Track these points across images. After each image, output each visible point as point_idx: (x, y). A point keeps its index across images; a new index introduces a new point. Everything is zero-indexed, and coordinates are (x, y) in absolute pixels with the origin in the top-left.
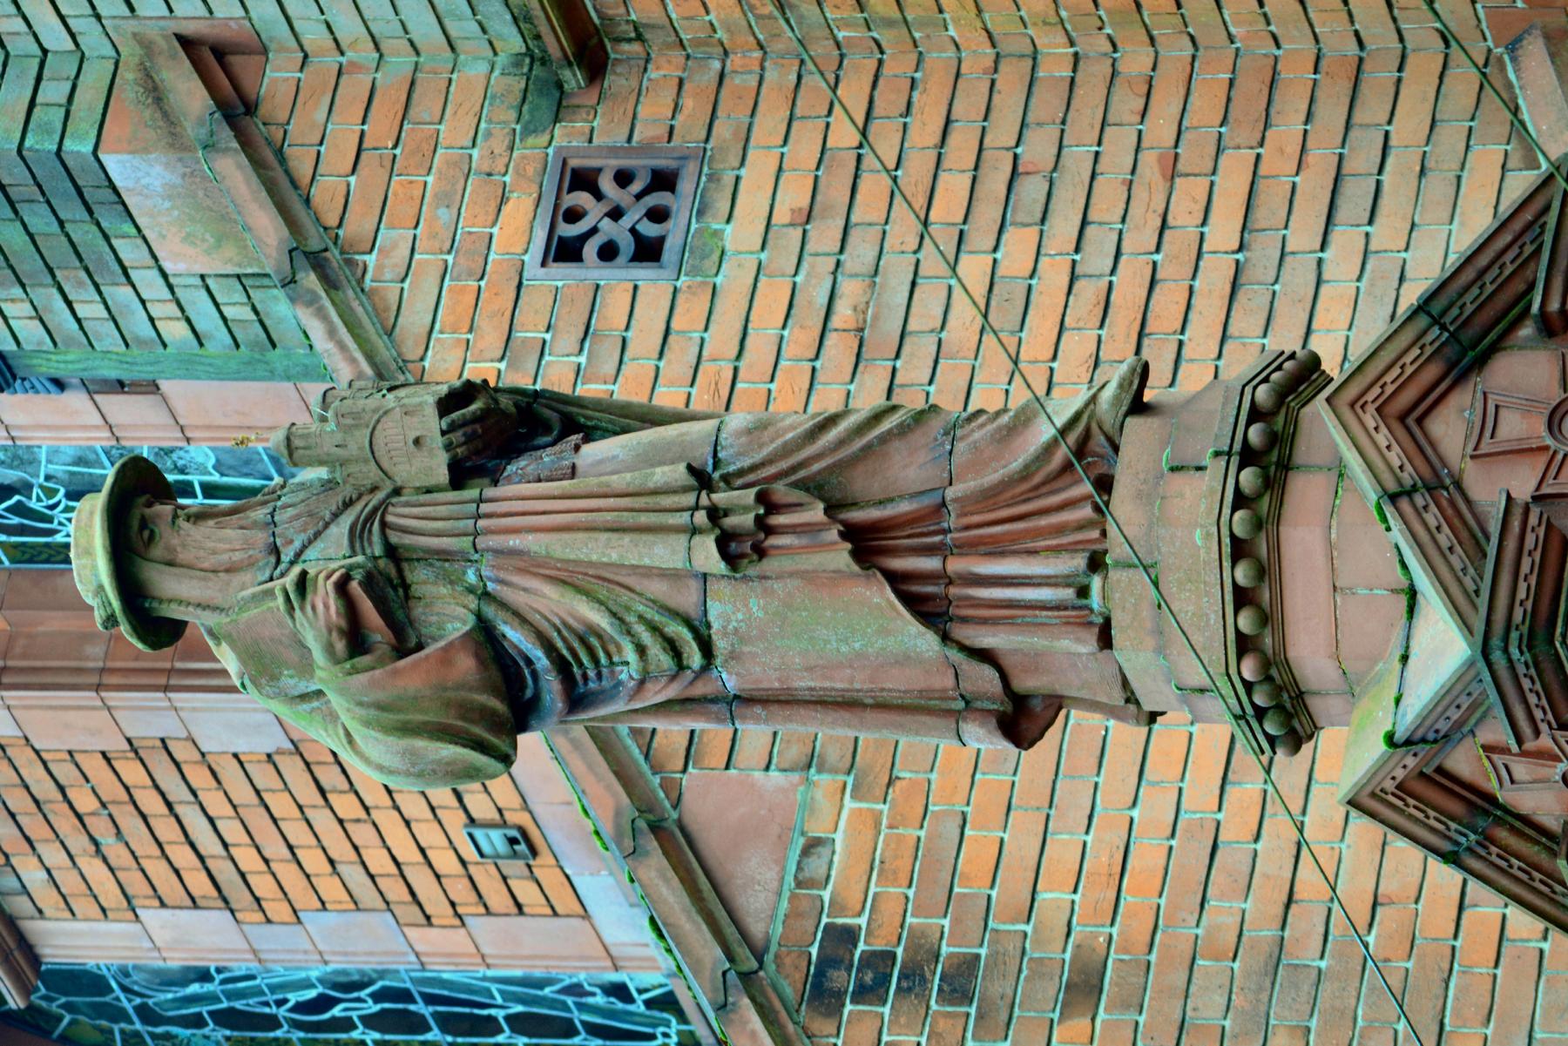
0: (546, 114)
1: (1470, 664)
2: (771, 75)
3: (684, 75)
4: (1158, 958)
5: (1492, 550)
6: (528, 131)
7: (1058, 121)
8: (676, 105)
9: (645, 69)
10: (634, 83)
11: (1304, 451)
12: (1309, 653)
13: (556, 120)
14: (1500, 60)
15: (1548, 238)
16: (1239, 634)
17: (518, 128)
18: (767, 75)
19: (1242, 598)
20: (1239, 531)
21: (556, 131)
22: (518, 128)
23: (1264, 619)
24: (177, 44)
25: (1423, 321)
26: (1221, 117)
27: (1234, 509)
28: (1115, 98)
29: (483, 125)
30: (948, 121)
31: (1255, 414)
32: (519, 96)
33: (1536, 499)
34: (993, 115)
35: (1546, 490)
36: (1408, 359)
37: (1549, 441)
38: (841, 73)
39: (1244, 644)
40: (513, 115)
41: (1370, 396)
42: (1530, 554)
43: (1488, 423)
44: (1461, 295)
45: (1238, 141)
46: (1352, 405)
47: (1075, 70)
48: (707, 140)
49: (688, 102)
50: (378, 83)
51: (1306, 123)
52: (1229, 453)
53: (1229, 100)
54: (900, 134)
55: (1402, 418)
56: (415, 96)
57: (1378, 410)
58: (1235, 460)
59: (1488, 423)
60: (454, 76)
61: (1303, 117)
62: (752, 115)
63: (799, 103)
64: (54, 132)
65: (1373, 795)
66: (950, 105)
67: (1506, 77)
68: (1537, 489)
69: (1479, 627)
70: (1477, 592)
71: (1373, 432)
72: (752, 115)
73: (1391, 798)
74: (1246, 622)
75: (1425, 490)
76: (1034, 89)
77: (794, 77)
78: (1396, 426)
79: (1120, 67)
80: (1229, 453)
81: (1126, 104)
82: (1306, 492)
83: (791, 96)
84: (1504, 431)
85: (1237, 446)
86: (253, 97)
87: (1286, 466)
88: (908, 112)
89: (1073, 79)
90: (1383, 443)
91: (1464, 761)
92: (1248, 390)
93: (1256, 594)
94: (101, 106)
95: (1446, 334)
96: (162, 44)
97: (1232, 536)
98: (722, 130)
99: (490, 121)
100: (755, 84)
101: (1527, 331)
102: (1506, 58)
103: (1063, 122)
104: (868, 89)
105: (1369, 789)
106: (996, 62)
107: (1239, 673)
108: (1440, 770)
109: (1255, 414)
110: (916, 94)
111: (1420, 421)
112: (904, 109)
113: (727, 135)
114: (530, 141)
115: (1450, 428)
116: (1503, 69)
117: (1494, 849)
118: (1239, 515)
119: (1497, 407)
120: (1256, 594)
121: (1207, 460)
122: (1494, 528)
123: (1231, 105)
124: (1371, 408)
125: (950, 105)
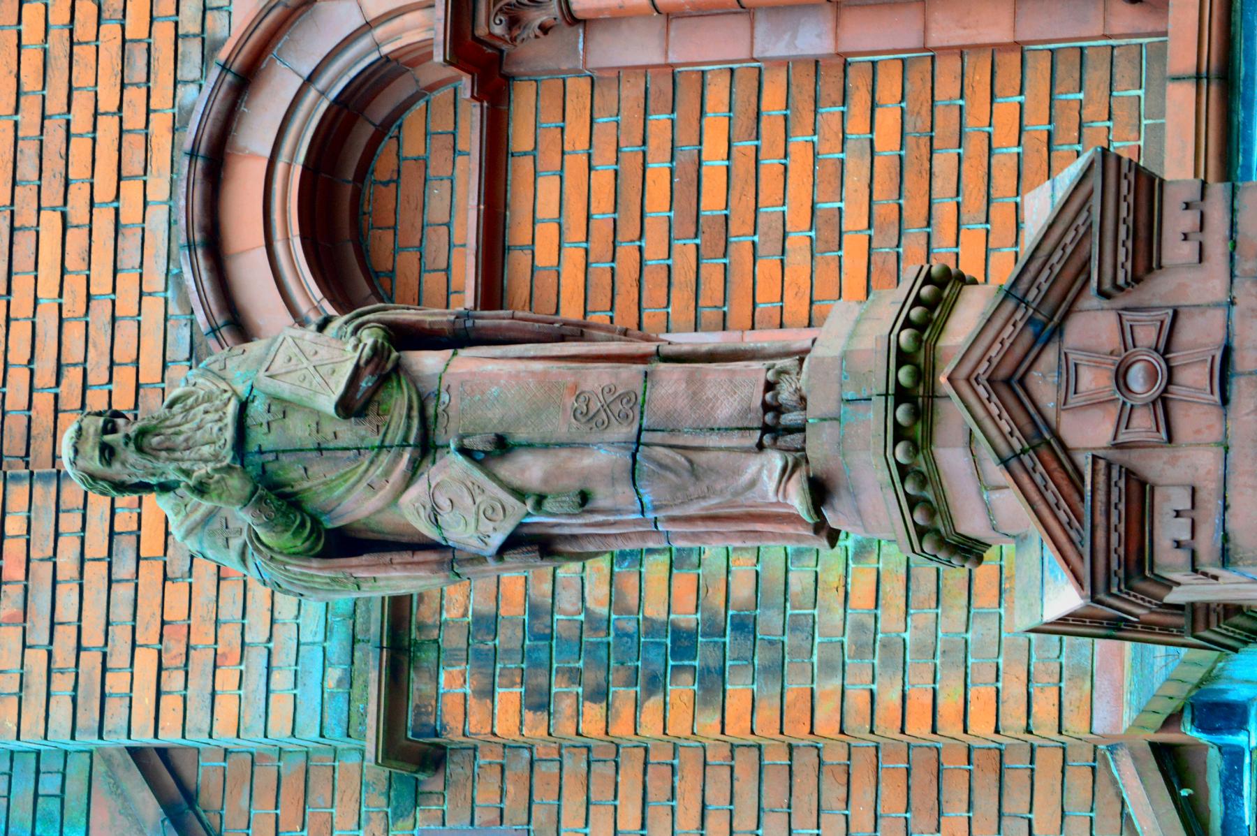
0: (409, 802)
2: (568, 763)
3: (504, 762)
4: (880, 659)
6: (398, 816)
7: (785, 806)
8: (502, 790)
9: (475, 757)
10: (469, 773)
13: (416, 804)
14: (1104, 757)
17: (389, 810)
18: (565, 762)
20: (901, 458)
21: (418, 815)
22: (389, 810)
23: (931, 512)
24: (129, 757)
25: (1010, 305)
26: (905, 805)
28: (823, 787)
29: (363, 809)
30: (704, 806)
31: (903, 358)
32: (386, 783)
34: (736, 800)
35: (1122, 438)
36: (1005, 334)
37: (1118, 395)
38: (619, 760)
40: (384, 800)
44: (1035, 278)
45: (921, 827)
47: (791, 760)
48: (529, 823)
49: (510, 788)
50: (282, 770)
51: (969, 811)
52: (887, 395)
53: (908, 788)
54: (670, 817)
56: (311, 783)
59: (1069, 375)
60: (337, 764)
61: (965, 807)
62: (559, 799)
63: (592, 788)
64: (52, 822)
66: (703, 791)
67: (1111, 773)
68: (1115, 438)
72: (559, 799)
74: (919, 517)
76: (763, 776)
77: (584, 765)
79: (825, 758)
80: (887, 395)
81: (833, 792)
83: (585, 783)
86: (194, 787)
88: (673, 797)
89: (790, 767)
92: (893, 337)
94: (86, 796)
96: (117, 756)
98: (539, 813)
99: (368, 806)
100: (557, 771)
101: (1090, 300)
102: (1108, 754)
103: (789, 807)
104: (640, 776)
106: (732, 751)
107: (898, 335)
110: (676, 779)
112: (669, 794)
113: (543, 818)
114: (400, 824)
116: (1107, 766)
119: (1076, 365)
123: (911, 793)
125: (703, 791)
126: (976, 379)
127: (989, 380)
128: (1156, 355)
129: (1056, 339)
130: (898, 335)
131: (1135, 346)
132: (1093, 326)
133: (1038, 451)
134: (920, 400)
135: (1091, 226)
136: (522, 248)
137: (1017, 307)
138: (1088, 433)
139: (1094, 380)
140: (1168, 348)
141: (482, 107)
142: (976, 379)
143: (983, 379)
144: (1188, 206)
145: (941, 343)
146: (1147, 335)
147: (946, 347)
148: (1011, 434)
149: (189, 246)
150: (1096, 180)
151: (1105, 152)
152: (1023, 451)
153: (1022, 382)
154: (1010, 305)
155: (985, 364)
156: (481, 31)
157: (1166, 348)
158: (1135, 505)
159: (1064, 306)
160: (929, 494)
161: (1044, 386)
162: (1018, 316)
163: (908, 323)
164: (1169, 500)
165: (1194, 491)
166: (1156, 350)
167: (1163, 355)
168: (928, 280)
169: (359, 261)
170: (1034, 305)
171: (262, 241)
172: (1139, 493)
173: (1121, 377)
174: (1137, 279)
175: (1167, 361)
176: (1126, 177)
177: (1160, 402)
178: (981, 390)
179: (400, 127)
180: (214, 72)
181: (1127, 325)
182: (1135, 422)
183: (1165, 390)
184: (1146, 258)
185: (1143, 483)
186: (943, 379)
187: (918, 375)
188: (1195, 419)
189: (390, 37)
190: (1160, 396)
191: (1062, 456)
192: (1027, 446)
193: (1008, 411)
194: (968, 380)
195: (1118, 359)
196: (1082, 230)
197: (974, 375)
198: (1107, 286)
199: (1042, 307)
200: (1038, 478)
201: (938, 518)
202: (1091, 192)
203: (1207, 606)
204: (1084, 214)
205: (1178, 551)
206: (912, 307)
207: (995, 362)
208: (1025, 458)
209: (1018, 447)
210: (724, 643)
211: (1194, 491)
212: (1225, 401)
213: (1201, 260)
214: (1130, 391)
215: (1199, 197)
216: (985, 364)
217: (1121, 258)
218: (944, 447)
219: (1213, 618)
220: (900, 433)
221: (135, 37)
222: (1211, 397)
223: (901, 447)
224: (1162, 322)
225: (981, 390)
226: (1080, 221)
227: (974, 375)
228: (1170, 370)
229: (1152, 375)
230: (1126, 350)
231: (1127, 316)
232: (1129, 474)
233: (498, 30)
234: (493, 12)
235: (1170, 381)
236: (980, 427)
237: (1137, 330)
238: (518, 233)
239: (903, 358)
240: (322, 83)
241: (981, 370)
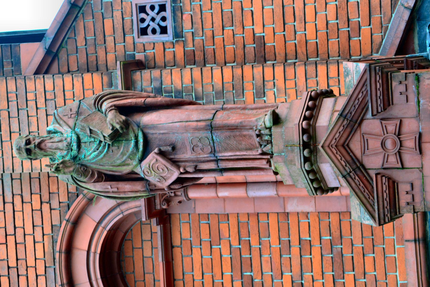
35: (385, 166)
42: (385, 184)
95: (349, 121)
107: (302, 124)
126: (331, 146)
127: (336, 146)
128: (395, 136)
129: (359, 129)
130: (302, 124)
131: (387, 133)
132: (371, 125)
133: (355, 170)
134: (312, 147)
135: (367, 92)
136: (180, 280)
137: (344, 121)
138: (373, 162)
139: (374, 144)
140: (399, 134)
141: (161, 227)
142: (331, 146)
143: (334, 146)
144: (407, 193)
145: (317, 125)
146: (391, 128)
147: (319, 126)
148: (346, 166)
149: (60, 252)
150: (367, 75)
152: (350, 172)
153: (348, 145)
155: (334, 141)
156: (158, 207)
157: (399, 134)
158: (391, 190)
159: (360, 118)
161: (356, 146)
163: (305, 118)
164: (403, 188)
166: (395, 134)
167: (397, 136)
168: (311, 99)
169: (121, 280)
170: (350, 119)
171: (88, 280)
172: (393, 185)
173: (383, 144)
174: (385, 109)
175: (399, 138)
176: (379, 82)
178: (334, 150)
179: (131, 230)
180: (64, 223)
181: (384, 126)
182: (390, 160)
183: (400, 149)
184: (387, 102)
185: (394, 182)
186: (320, 147)
187: (310, 137)
188: (410, 159)
191: (363, 171)
192: (352, 170)
193: (343, 157)
194: (329, 146)
195: (382, 138)
196: (365, 93)
197: (331, 145)
198: (375, 113)
199: (352, 120)
200: (356, 181)
202: (366, 80)
205: (408, 195)
206: (306, 112)
207: (338, 139)
208: (351, 174)
209: (348, 171)
212: (421, 152)
213: (407, 101)
214: (386, 148)
215: (412, 201)
216: (334, 141)
217: (379, 103)
218: (321, 163)
220: (306, 160)
222: (416, 151)
223: (304, 123)
224: (396, 125)
225: (334, 150)
226: (363, 89)
227: (331, 145)
228: (401, 142)
229: (395, 143)
230: (384, 135)
231: (383, 122)
232: (389, 179)
233: (164, 207)
234: (162, 200)
235: (401, 146)
238: (178, 274)
239: (304, 131)
240: (103, 224)
241: (333, 143)
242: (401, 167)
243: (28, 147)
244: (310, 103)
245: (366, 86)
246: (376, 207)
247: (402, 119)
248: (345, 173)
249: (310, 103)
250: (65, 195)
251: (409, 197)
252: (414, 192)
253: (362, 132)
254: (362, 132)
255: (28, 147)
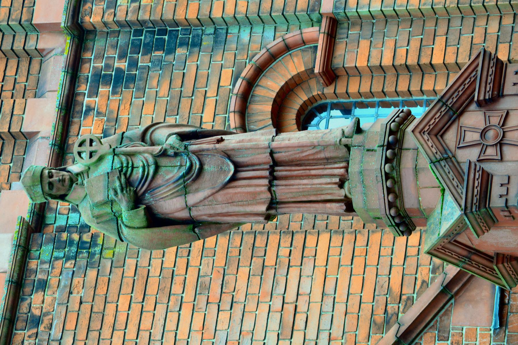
1: (461, 215)
5: (466, 178)
11: (406, 145)
12: (410, 202)
15: (479, 73)
16: (386, 173)
19: (389, 191)
25: (440, 104)
27: (390, 209)
33: (478, 161)
35: (481, 158)
39: (391, 205)
41: (426, 129)
42: (477, 180)
43: (461, 137)
46: (420, 132)
55: (436, 135)
57: (428, 134)
58: (385, 148)
59: (461, 137)
65: (435, 250)
69: (463, 206)
70: (462, 193)
71: (427, 141)
73: (440, 250)
75: (445, 159)
78: (435, 139)
82: (407, 161)
84: (467, 139)
85: (386, 143)
87: (401, 149)
90: (430, 145)
91: (463, 239)
93: (394, 187)
95: (448, 108)
97: (387, 187)
101: (473, 106)
105: (433, 249)
108: (455, 241)
109: (391, 133)
111: (442, 136)
115: (451, 137)
117: (474, 263)
118: (387, 165)
120: (394, 187)
121: (376, 148)
122: (466, 170)
124: (426, 133)
129: (457, 120)
132: (473, 118)
138: (468, 156)
146: (495, 121)
151: (485, 51)
154: (440, 104)
160: (394, 174)
162: (443, 109)
165: (509, 177)
172: (487, 179)
177: (499, 145)
183: (501, 140)
184: (498, 94)
189: (253, 165)
190: (499, 142)
199: (451, 109)
201: (395, 172)
202: (478, 65)
203: (504, 255)
204: (474, 73)
210: (189, 38)
211: (509, 177)
219: (505, 260)
221: (278, 313)
236: (422, 145)
237: (491, 118)
242: (500, 158)
243: (51, 180)
244: (391, 138)
245: (477, 71)
246: (464, 196)
247: (509, 111)
248: (434, 159)
249: (391, 138)
250: (105, 191)
251: (504, 189)
252: (508, 197)
253: (460, 125)
254: (460, 125)
255: (51, 180)
